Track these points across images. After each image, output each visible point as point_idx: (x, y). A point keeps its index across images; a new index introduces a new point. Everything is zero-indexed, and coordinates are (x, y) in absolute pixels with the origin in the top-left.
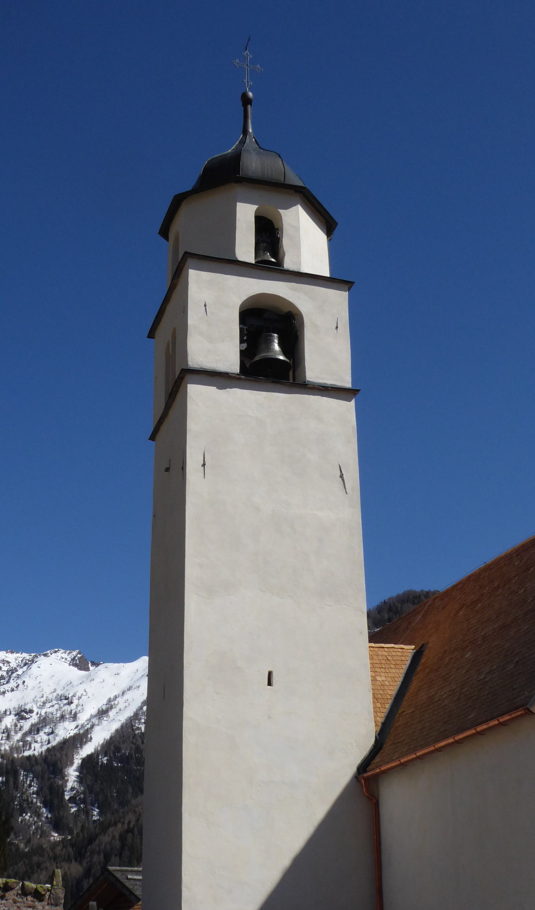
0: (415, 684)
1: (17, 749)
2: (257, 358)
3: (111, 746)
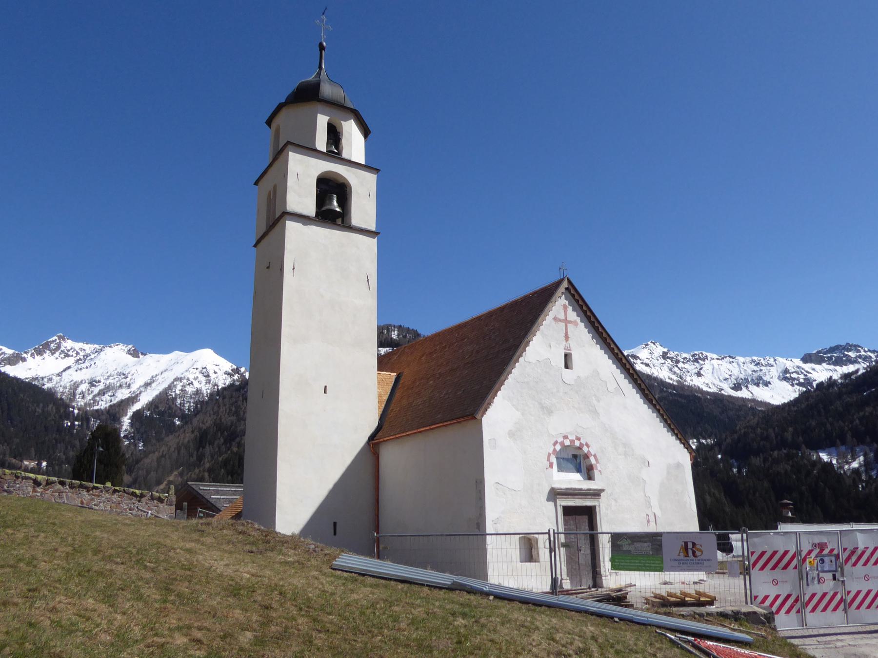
0: (398, 394)
1: (90, 405)
2: (324, 209)
3: (153, 405)
